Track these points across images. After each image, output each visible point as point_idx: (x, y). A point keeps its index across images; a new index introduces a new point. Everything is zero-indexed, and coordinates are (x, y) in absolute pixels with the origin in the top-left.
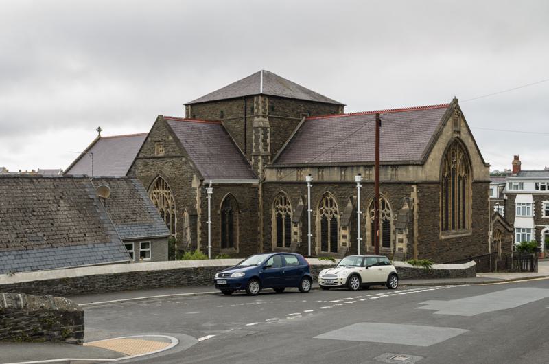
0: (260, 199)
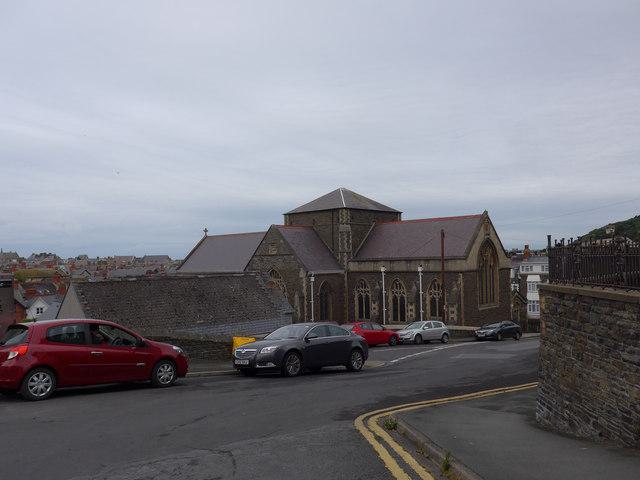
0: (346, 284)
